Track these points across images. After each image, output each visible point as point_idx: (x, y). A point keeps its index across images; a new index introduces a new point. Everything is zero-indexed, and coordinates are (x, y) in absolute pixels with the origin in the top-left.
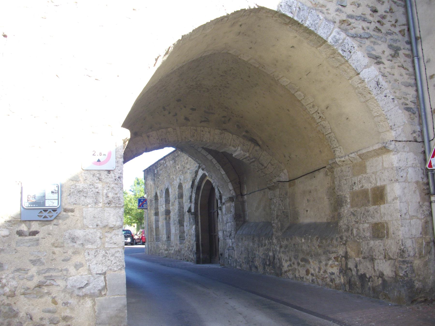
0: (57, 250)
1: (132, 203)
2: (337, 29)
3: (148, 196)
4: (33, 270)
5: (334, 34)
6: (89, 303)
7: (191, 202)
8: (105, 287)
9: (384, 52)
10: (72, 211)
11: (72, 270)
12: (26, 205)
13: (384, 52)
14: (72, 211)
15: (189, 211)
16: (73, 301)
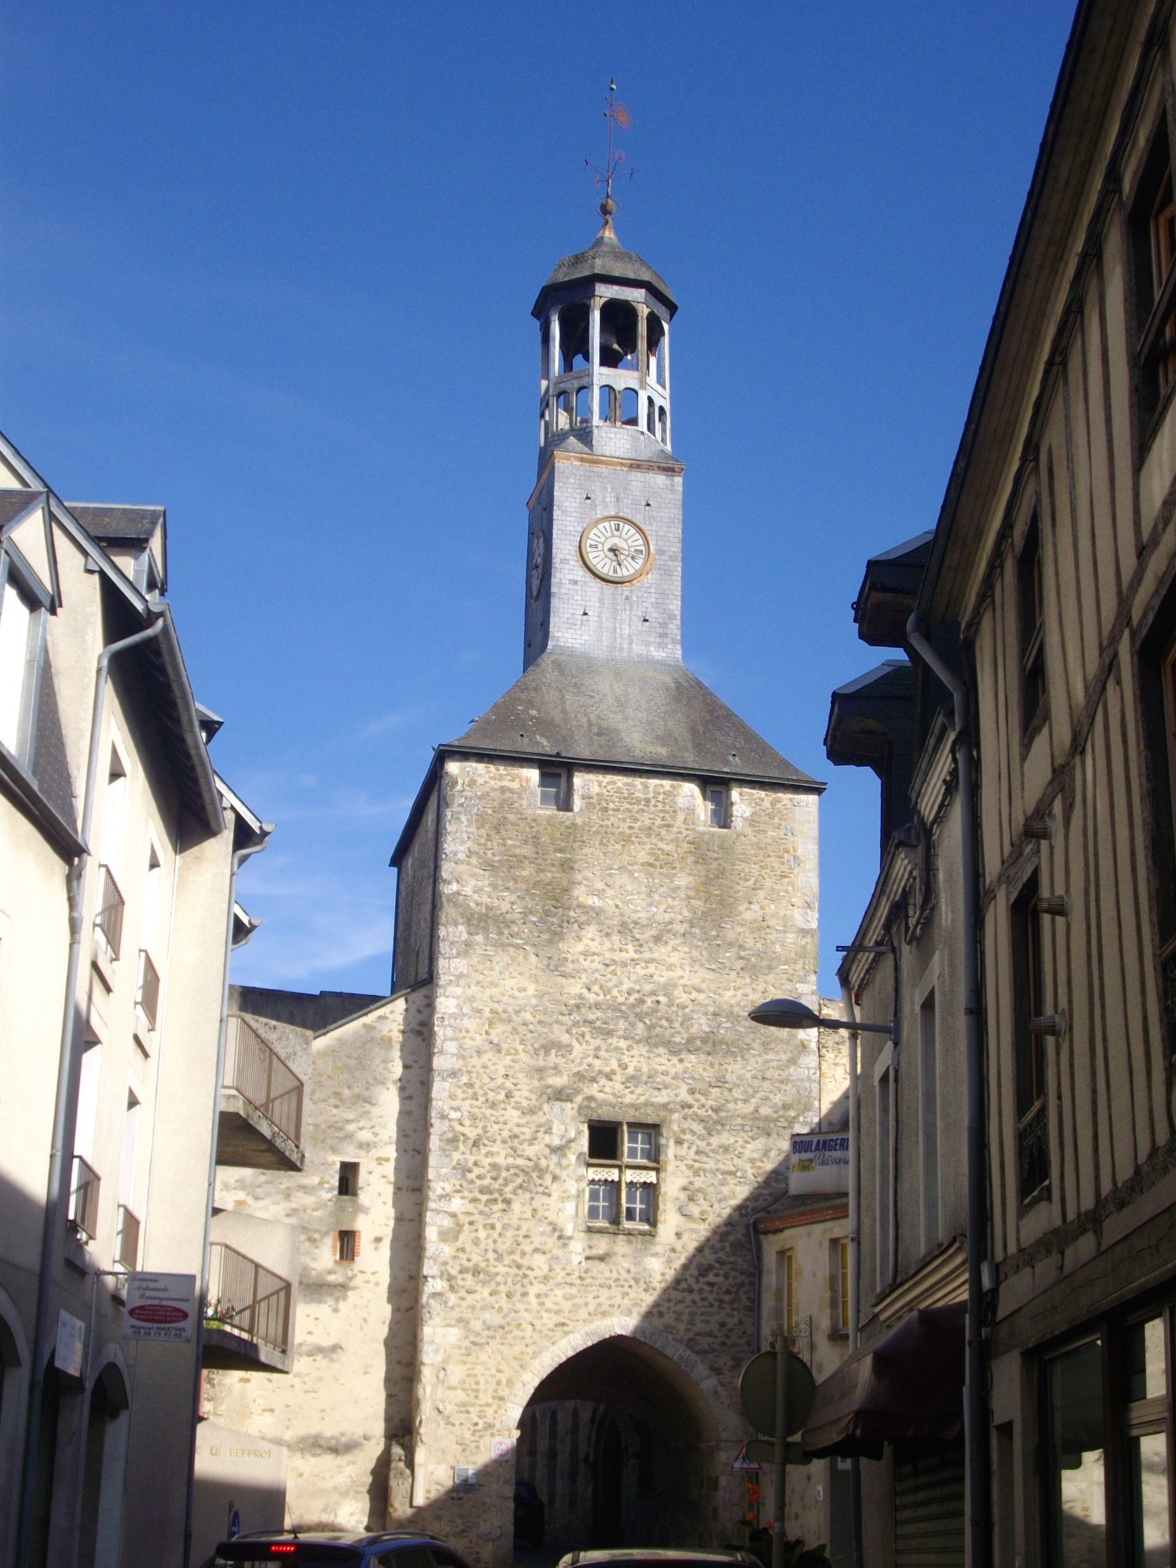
2: (683, 1348)
5: (680, 1352)
6: (490, 1545)
7: (589, 1445)
9: (725, 1364)
11: (482, 1523)
12: (457, 1481)
13: (725, 1364)
14: (483, 1486)
15: (586, 1459)
16: (481, 1542)
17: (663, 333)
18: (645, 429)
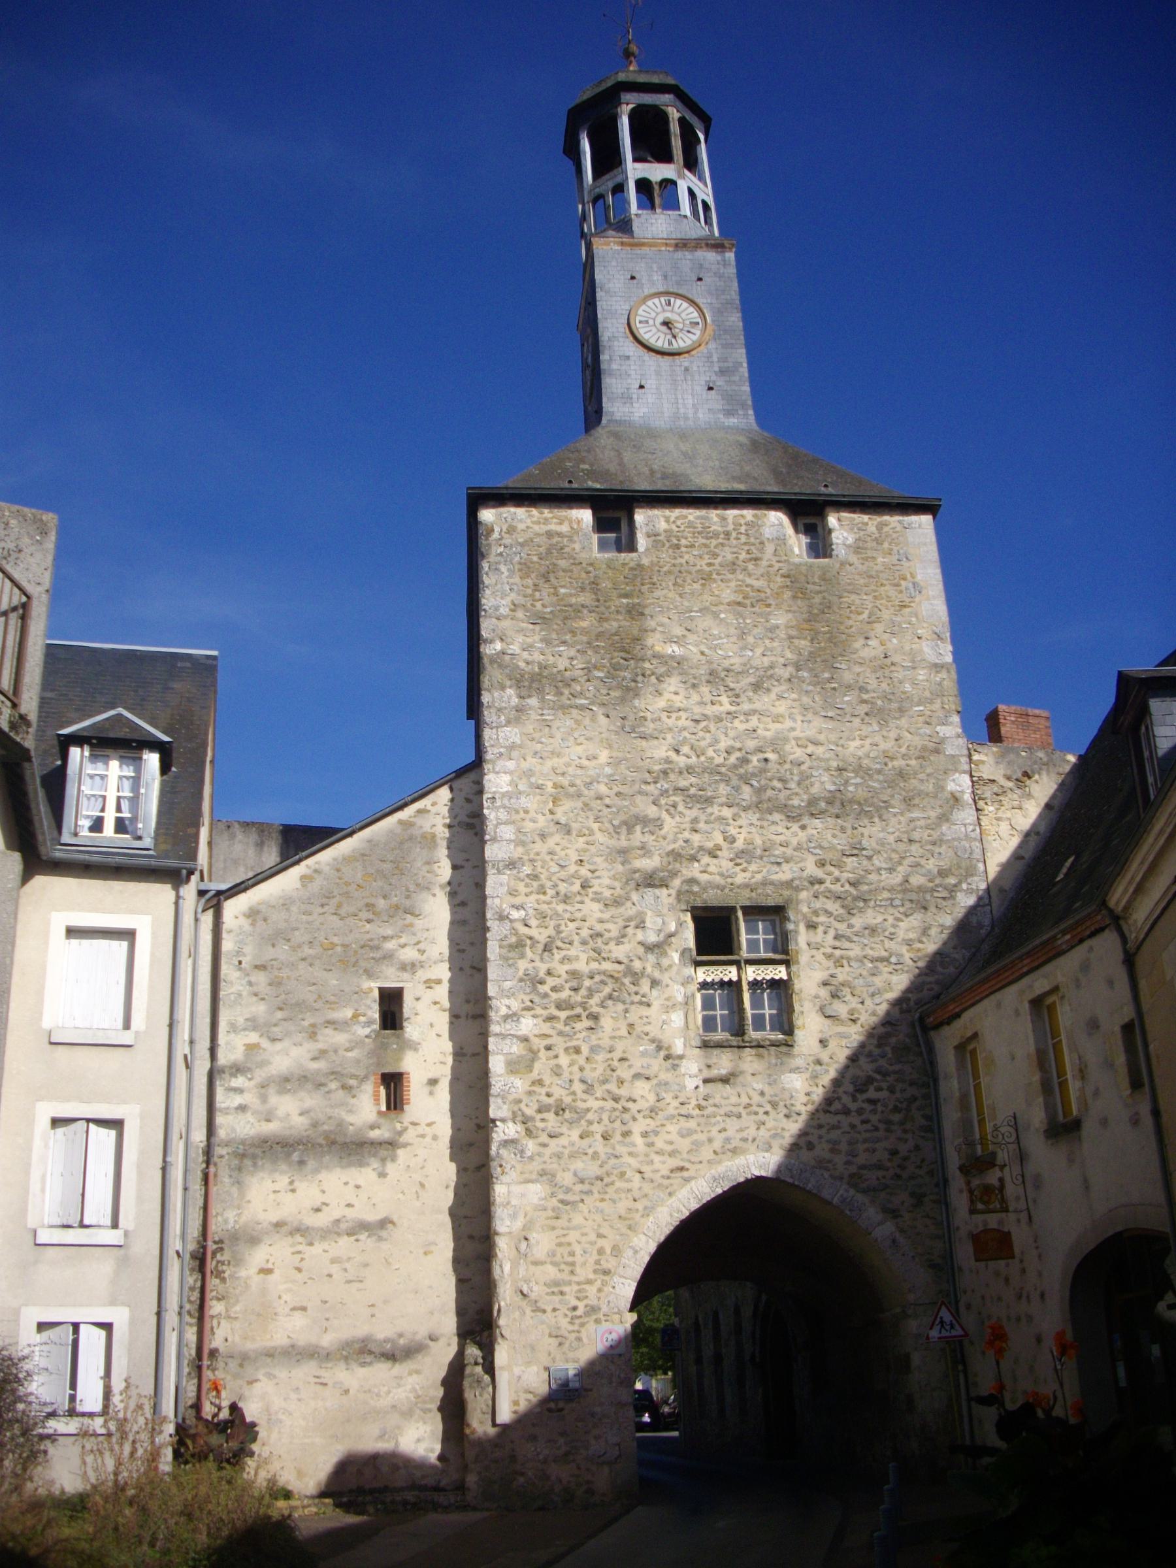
0: (579, 1424)
1: (653, 1313)
2: (845, 1186)
3: (681, 1322)
4: (562, 1440)
5: (841, 1192)
6: (606, 1469)
8: (620, 1456)
9: (903, 1203)
10: (591, 1390)
14: (591, 1390)
17: (699, 141)
18: (688, 213)
